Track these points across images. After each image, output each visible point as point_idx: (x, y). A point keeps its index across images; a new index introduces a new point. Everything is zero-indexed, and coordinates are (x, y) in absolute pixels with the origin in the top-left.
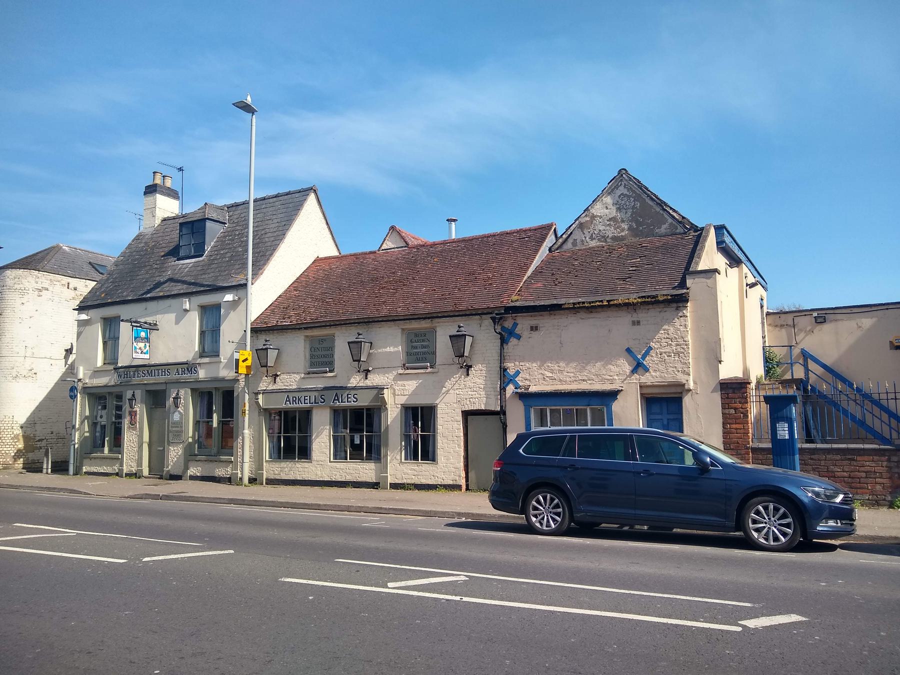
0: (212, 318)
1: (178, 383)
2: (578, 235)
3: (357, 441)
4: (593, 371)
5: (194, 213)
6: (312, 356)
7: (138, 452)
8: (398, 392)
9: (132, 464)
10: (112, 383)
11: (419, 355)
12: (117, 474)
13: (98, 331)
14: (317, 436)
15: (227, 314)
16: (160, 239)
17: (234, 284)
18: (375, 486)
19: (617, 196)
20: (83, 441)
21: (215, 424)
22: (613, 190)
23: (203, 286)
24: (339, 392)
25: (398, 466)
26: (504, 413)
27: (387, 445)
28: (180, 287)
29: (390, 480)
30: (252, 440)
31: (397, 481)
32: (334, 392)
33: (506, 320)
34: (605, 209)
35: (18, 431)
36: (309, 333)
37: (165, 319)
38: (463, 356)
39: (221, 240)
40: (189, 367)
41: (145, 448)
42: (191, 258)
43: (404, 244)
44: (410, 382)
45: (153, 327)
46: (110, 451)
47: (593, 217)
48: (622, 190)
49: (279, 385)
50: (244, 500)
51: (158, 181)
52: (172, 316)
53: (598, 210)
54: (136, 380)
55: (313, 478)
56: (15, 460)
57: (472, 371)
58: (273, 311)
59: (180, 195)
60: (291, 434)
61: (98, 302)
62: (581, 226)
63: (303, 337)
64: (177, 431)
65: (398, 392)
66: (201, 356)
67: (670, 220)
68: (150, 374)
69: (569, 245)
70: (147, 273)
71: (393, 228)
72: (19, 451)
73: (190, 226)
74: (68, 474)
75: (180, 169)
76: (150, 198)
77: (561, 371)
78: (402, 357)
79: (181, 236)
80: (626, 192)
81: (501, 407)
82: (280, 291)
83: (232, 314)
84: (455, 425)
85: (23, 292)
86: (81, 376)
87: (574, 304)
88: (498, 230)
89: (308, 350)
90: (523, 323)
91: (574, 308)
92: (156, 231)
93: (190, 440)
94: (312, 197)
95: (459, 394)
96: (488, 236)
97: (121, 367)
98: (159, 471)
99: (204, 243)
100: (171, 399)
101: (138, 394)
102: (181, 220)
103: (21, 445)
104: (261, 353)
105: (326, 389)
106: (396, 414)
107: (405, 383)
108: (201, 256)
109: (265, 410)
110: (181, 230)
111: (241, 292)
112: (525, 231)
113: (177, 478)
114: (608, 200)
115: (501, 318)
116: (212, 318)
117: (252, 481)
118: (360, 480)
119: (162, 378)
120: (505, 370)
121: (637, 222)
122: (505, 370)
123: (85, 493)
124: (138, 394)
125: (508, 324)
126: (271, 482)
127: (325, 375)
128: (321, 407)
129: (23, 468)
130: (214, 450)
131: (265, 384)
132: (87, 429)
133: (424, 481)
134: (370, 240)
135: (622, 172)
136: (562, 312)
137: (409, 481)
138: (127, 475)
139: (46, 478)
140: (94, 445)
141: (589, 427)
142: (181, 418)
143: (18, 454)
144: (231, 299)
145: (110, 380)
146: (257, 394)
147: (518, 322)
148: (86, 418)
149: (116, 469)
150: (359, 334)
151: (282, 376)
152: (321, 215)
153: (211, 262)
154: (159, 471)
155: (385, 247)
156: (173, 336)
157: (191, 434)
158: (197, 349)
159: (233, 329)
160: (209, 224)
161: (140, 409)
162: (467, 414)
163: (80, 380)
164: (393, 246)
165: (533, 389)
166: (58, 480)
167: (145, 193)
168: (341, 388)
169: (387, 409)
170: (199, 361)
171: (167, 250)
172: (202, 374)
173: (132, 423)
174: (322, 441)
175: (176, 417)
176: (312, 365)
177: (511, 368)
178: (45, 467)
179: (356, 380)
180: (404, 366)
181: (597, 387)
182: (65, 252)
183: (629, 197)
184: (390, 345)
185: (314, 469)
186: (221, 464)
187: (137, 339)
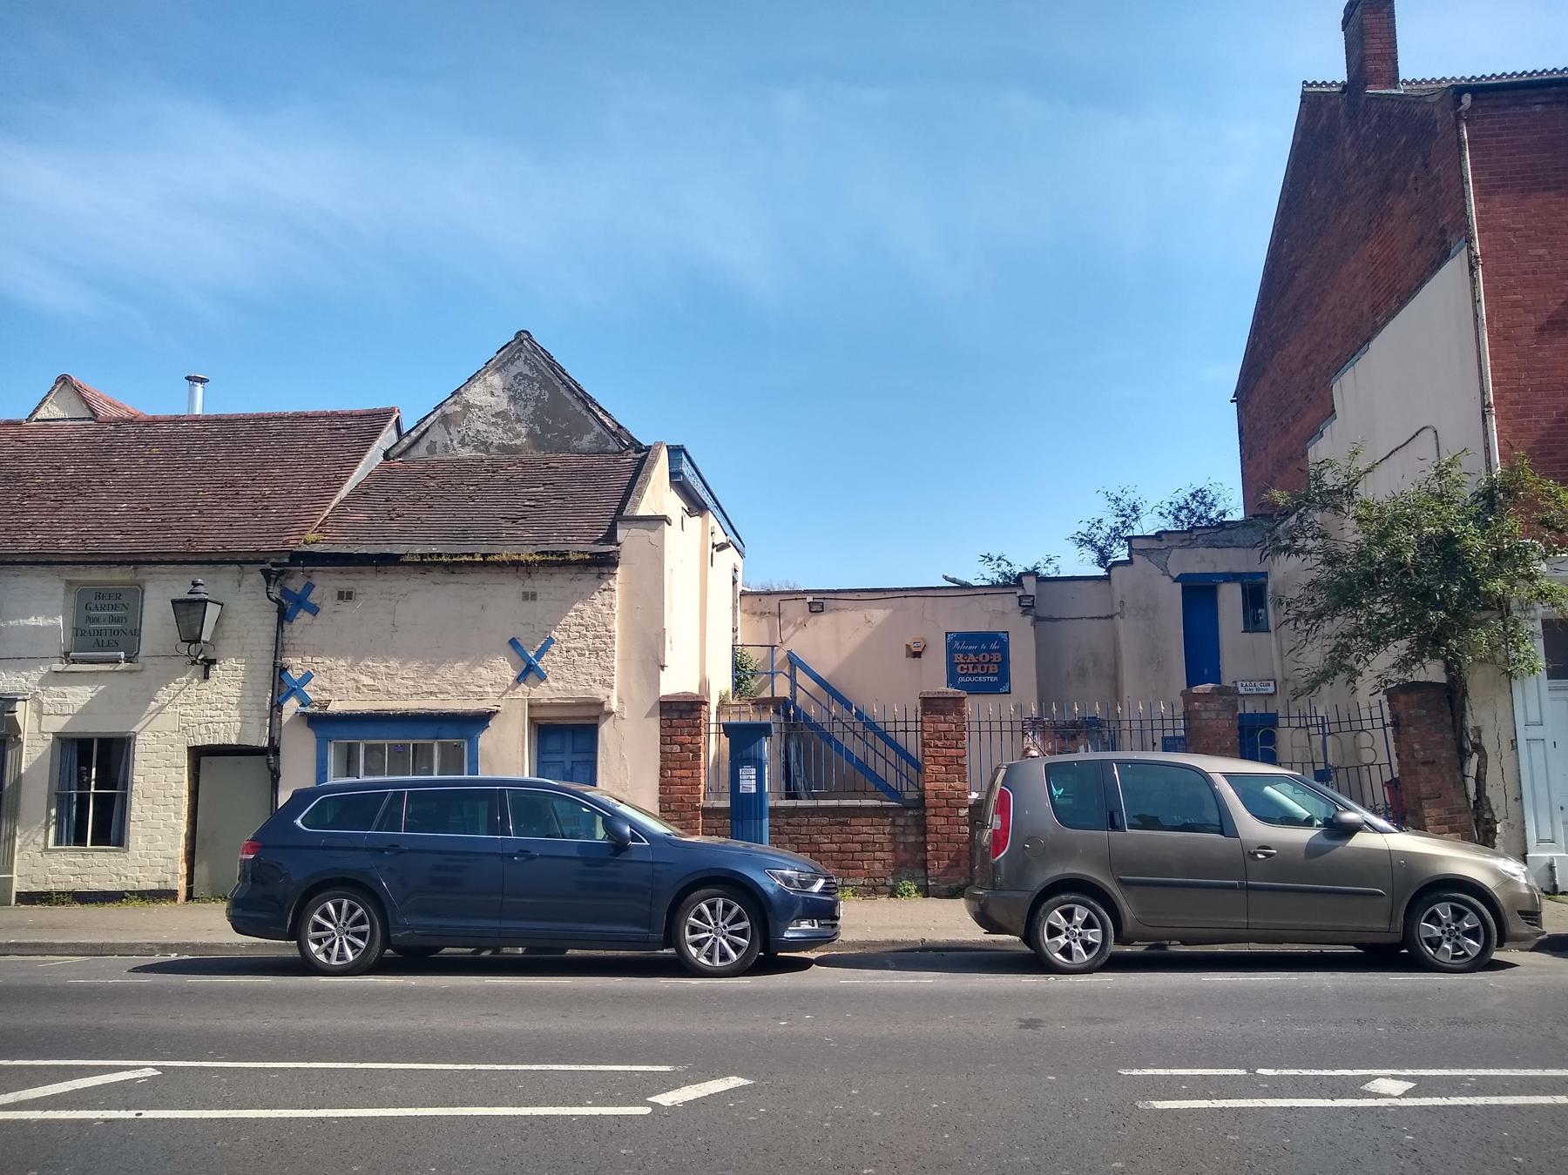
2: (438, 435)
4: (449, 676)
11: (103, 635)
22: (505, 365)
25: (39, 859)
26: (276, 752)
31: (34, 888)
33: (291, 578)
34: (489, 395)
36: (97, 575)
38: (197, 640)
43: (88, 414)
44: (78, 689)
47: (468, 407)
48: (520, 367)
53: (476, 395)
57: (216, 671)
67: (598, 428)
69: (420, 451)
71: (64, 380)
77: (390, 676)
78: (63, 639)
80: (526, 371)
81: (271, 739)
90: (325, 585)
91: (421, 563)
107: (67, 690)
114: (496, 380)
115: (281, 573)
120: (283, 670)
121: (542, 424)
125: (296, 585)
133: (95, 886)
135: (523, 337)
137: (62, 887)
155: (38, 416)
162: (199, 755)
164: (62, 415)
165: (335, 707)
169: (20, 742)
177: (296, 666)
180: (66, 657)
181: (455, 705)
183: (532, 380)
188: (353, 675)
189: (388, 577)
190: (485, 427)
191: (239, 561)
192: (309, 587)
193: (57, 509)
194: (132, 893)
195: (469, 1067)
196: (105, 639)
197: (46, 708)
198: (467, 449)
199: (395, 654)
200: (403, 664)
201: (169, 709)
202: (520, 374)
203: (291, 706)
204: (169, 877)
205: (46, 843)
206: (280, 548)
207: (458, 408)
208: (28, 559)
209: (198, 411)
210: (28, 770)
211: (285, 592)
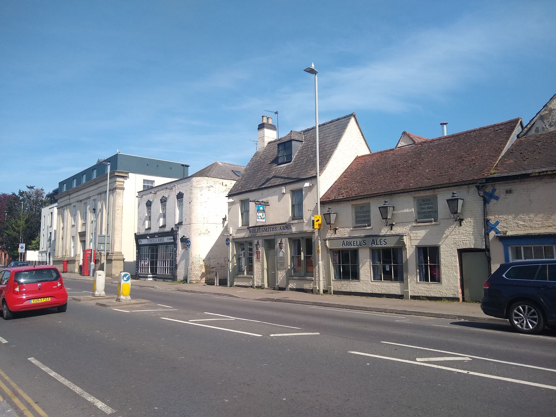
0: (298, 195)
1: (281, 235)
2: (539, 124)
5: (285, 137)
6: (356, 217)
8: (413, 238)
10: (247, 236)
11: (426, 214)
12: (251, 287)
13: (238, 208)
14: (362, 266)
15: (306, 194)
18: (400, 297)
20: (234, 268)
21: (302, 258)
24: (375, 238)
25: (415, 285)
27: (407, 272)
29: (410, 294)
30: (324, 268)
31: (415, 295)
32: (372, 239)
33: (487, 188)
35: (202, 263)
36: (354, 203)
37: (273, 199)
39: (301, 152)
40: (287, 226)
43: (412, 143)
44: (421, 231)
45: (266, 204)
46: (247, 273)
47: (551, 110)
49: (338, 235)
51: (265, 121)
52: (276, 197)
54: (259, 234)
57: (464, 223)
61: (238, 192)
65: (413, 238)
66: (293, 219)
68: (266, 231)
69: (533, 132)
71: (404, 133)
73: (283, 145)
75: (276, 113)
76: (261, 132)
77: (531, 221)
78: (415, 215)
79: (279, 151)
81: (486, 246)
82: (335, 179)
85: (201, 189)
86: (231, 233)
87: (539, 173)
88: (477, 127)
90: (500, 189)
91: (539, 176)
93: (289, 267)
94: (353, 119)
95: (455, 239)
98: (273, 286)
99: (291, 154)
101: (260, 242)
102: (278, 142)
103: (204, 271)
104: (326, 216)
106: (412, 252)
107: (418, 232)
109: (330, 249)
111: (313, 181)
116: (298, 195)
117: (325, 292)
118: (391, 293)
119: (273, 233)
120: (488, 221)
123: (236, 297)
125: (489, 190)
126: (336, 293)
132: (235, 262)
133: (433, 295)
134: (390, 142)
137: (423, 295)
139: (216, 288)
140: (239, 270)
142: (284, 255)
143: (203, 275)
144: (308, 185)
146: (325, 240)
148: (235, 255)
151: (339, 229)
153: (296, 165)
154: (273, 286)
155: (399, 145)
156: (277, 209)
159: (310, 203)
160: (294, 143)
161: (261, 250)
162: (461, 252)
164: (405, 144)
165: (509, 233)
167: (259, 129)
168: (376, 236)
169: (406, 249)
171: (271, 160)
172: (294, 229)
173: (258, 258)
174: (366, 269)
175: (281, 254)
176: (357, 222)
177: (493, 219)
179: (385, 231)
182: (220, 166)
184: (406, 208)
187: (258, 211)
188: (515, 221)
192: (494, 190)
198: (553, 127)
200: (536, 216)
207: (547, 112)
211: (485, 193)
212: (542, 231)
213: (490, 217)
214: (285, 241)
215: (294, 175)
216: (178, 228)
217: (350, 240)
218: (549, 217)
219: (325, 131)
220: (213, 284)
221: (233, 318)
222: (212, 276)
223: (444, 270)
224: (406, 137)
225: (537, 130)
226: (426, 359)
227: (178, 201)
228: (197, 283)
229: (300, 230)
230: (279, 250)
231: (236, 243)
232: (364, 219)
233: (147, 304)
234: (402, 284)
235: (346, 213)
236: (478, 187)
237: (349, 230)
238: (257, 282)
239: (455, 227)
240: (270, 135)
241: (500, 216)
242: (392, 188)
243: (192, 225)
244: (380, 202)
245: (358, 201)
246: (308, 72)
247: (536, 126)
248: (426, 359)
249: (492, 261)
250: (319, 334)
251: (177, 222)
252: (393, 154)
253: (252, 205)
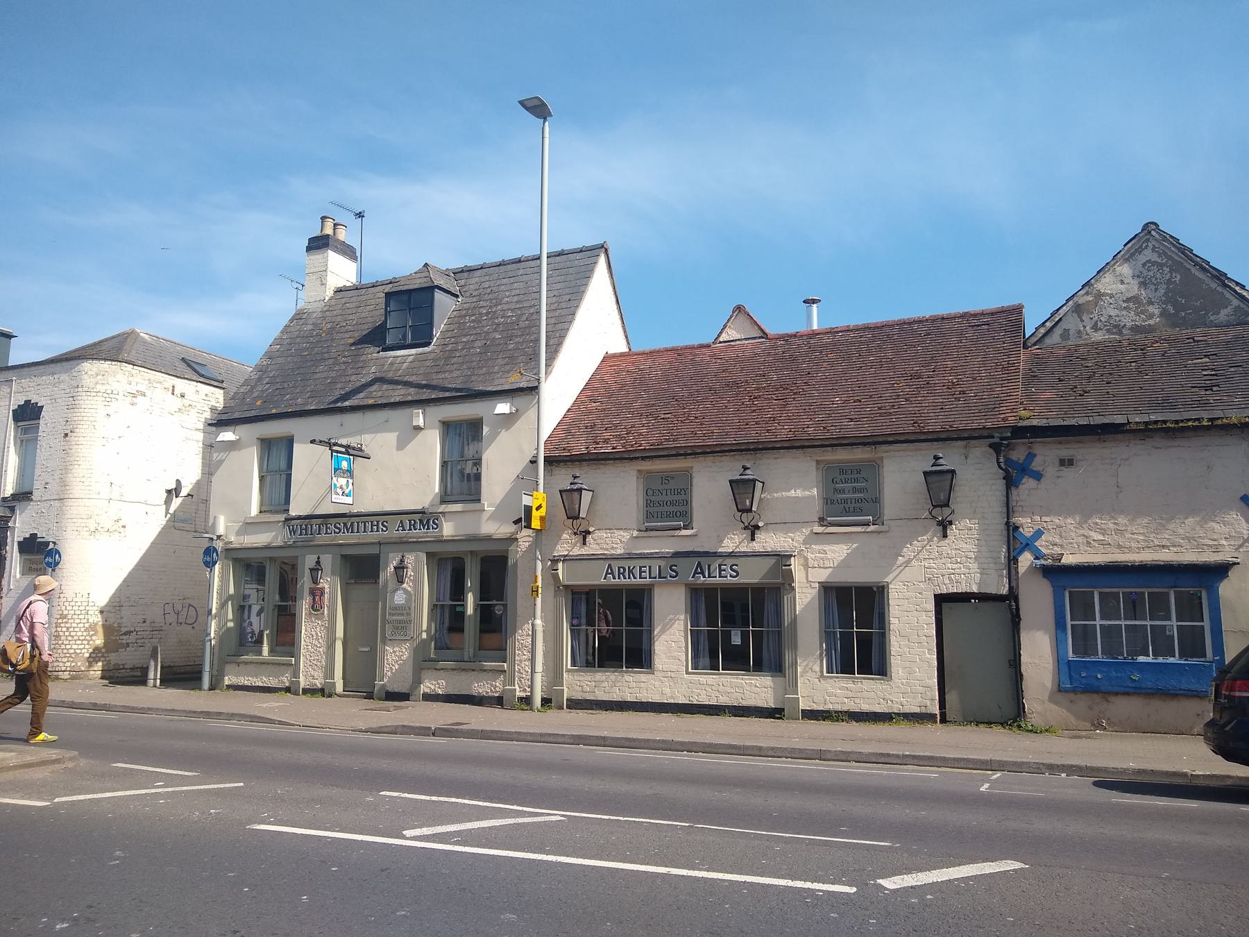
0: (464, 440)
1: (403, 544)
2: (1071, 324)
3: (736, 640)
4: (1181, 531)
5: (409, 277)
6: (648, 503)
7: (326, 654)
8: (816, 563)
9: (316, 674)
10: (279, 542)
11: (851, 502)
12: (288, 690)
13: (249, 463)
14: (663, 631)
15: (494, 435)
16: (339, 319)
17: (506, 387)
18: (775, 713)
19: (1140, 264)
20: (224, 636)
21: (470, 610)
22: (1132, 255)
23: (448, 390)
24: (703, 560)
25: (816, 684)
26: (1016, 599)
27: (794, 647)
28: (402, 392)
29: (803, 705)
30: (540, 636)
31: (815, 707)
32: (695, 561)
33: (1015, 450)
34: (1120, 283)
35: (97, 619)
36: (842, 455)
37: (379, 440)
38: (577, 517)
39: (458, 320)
40: (424, 518)
41: (339, 646)
42: (417, 343)
43: (758, 334)
44: (836, 547)
45: (354, 452)
46: (271, 651)
47: (1099, 295)
48: (1148, 255)
49: (592, 548)
50: (604, 738)
51: (329, 230)
52: (391, 438)
53: (1107, 284)
54: (322, 539)
55: (656, 698)
56: (90, 665)
57: (953, 531)
58: (568, 432)
59: (358, 254)
60: (612, 627)
61: (253, 413)
62: (1078, 309)
63: (635, 473)
64: (400, 622)
65: (816, 563)
66: (443, 502)
67: (1236, 302)
69: (1055, 338)
70: (331, 369)
71: (739, 309)
72: (96, 649)
73: (405, 297)
74: (200, 689)
75: (360, 215)
76: (317, 257)
77: (1119, 532)
78: (816, 509)
79: (387, 313)
80: (1155, 258)
81: (1011, 588)
82: (568, 404)
83: (504, 435)
84: (923, 617)
85: (110, 397)
86: (221, 530)
87: (1146, 423)
88: (927, 312)
89: (641, 493)
90: (1046, 455)
91: (1147, 430)
92: (329, 307)
93: (424, 636)
94: (602, 259)
95: (925, 570)
96: (911, 323)
97: (299, 518)
98: (363, 683)
99: (430, 325)
100: (307, 572)
101: (327, 560)
102: (388, 289)
103: (99, 641)
104: (571, 495)
105: (677, 555)
106: (809, 597)
107: (827, 548)
108: (428, 344)
109: (566, 587)
110: (387, 305)
111: (521, 401)
112: (975, 315)
113: (403, 697)
114: (1125, 270)
115: (1008, 445)
116: (464, 440)
117: (546, 702)
118: (745, 703)
119: (373, 536)
120: (1016, 528)
121: (1175, 304)
122: (1016, 528)
123: (281, 723)
124: (327, 560)
125: (1018, 455)
126: (575, 704)
127: (677, 533)
128: (668, 583)
129: (102, 678)
130: (469, 651)
131: (566, 545)
132: (230, 616)
133: (866, 707)
134: (698, 325)
135: (1150, 228)
136: (1119, 436)
137: (839, 708)
138: (305, 691)
139: (153, 695)
140: (241, 642)
141: (1206, 624)
142: (408, 600)
143: (96, 655)
144: (507, 411)
145: (276, 537)
146: (555, 561)
147: (1035, 451)
148: (230, 597)
149: (286, 680)
150: (575, 478)
151: (598, 534)
152: (611, 289)
153: (447, 355)
154: (363, 683)
155: (724, 337)
156: (396, 469)
157: (425, 627)
158: (437, 490)
159: (504, 460)
160: (438, 295)
161: (330, 584)
162: (942, 600)
163: (219, 537)
164: (738, 337)
165: (1068, 560)
166: (176, 697)
167: (309, 249)
168: (706, 554)
169: (793, 589)
170: (442, 508)
171: (357, 335)
173: (316, 607)
174: (672, 639)
175: (399, 598)
176: (649, 516)
177: (1027, 525)
178: (151, 675)
179: (733, 542)
180: (822, 521)
181: (1189, 556)
182: (145, 342)
183: (1161, 265)
184: (794, 487)
185: (657, 683)
186: (482, 675)
187: (337, 470)
188: (1082, 532)
189: (1106, 444)
190: (1117, 312)
191: (795, 445)
192: (1031, 456)
193: (785, 406)
194: (898, 714)
195: (150, 769)
196: (852, 506)
197: (811, 563)
198: (1100, 333)
199: (1122, 512)
200: (1132, 521)
201: (914, 563)
202: (1149, 261)
203: (1026, 560)
204: (928, 703)
205: (822, 672)
206: (1002, 424)
207: (1090, 298)
208: (786, 445)
209: (815, 327)
210: (803, 611)
211: (1008, 461)
212: (1147, 557)
213: (1018, 520)
214: (416, 563)
215: (453, 378)
216: (12, 509)
217: (631, 563)
218: (1163, 526)
219: (525, 278)
220: (138, 678)
221: (556, 816)
222: (128, 658)
223: (898, 647)
224: (742, 317)
225: (1065, 335)
226: (426, 831)
227: (17, 427)
228: (73, 678)
229: (470, 530)
230: (391, 587)
231: (236, 561)
232: (671, 509)
233: (70, 765)
234: (780, 680)
235: (618, 495)
236: (997, 448)
237: (626, 536)
238: (309, 674)
239: (930, 540)
240: (341, 271)
241: (1044, 519)
242: (752, 435)
243: (70, 503)
244: (730, 469)
245: (657, 461)
246: (527, 109)
247: (1063, 325)
248: (426, 831)
249: (1022, 624)
250: (1017, 865)
251: (9, 491)
252: (713, 356)
253: (301, 451)
